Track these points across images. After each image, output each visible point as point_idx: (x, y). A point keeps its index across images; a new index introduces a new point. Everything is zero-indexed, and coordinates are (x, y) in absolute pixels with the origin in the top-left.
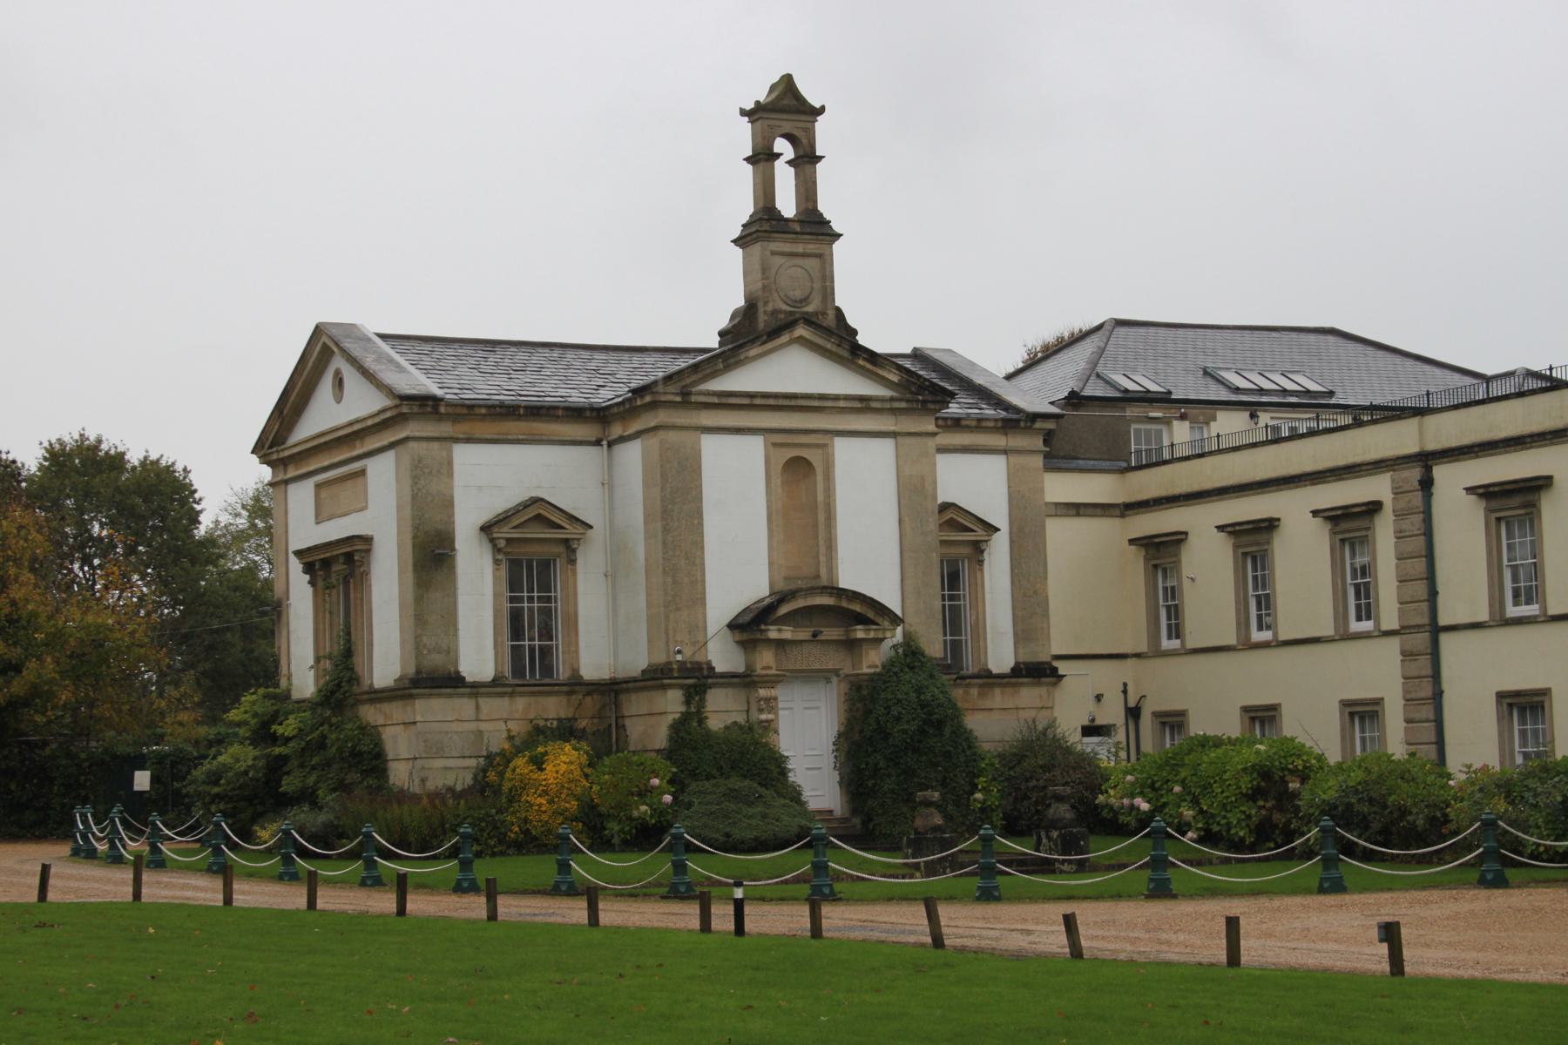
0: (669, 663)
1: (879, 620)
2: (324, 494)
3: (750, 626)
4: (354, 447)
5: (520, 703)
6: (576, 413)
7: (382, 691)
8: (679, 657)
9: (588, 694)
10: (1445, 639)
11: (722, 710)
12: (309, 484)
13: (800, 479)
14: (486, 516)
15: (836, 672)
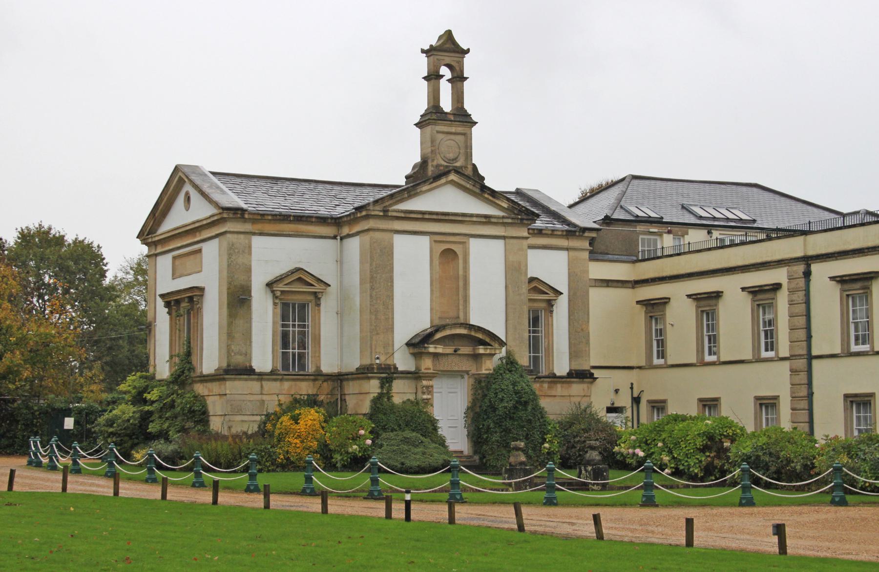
0: (371, 364)
1: (493, 343)
2: (177, 262)
3: (418, 345)
4: (195, 236)
5: (286, 385)
6: (323, 220)
7: (208, 376)
8: (378, 361)
9: (325, 381)
10: (815, 363)
11: (402, 392)
12: (169, 257)
13: (449, 261)
14: (269, 278)
15: (467, 372)
